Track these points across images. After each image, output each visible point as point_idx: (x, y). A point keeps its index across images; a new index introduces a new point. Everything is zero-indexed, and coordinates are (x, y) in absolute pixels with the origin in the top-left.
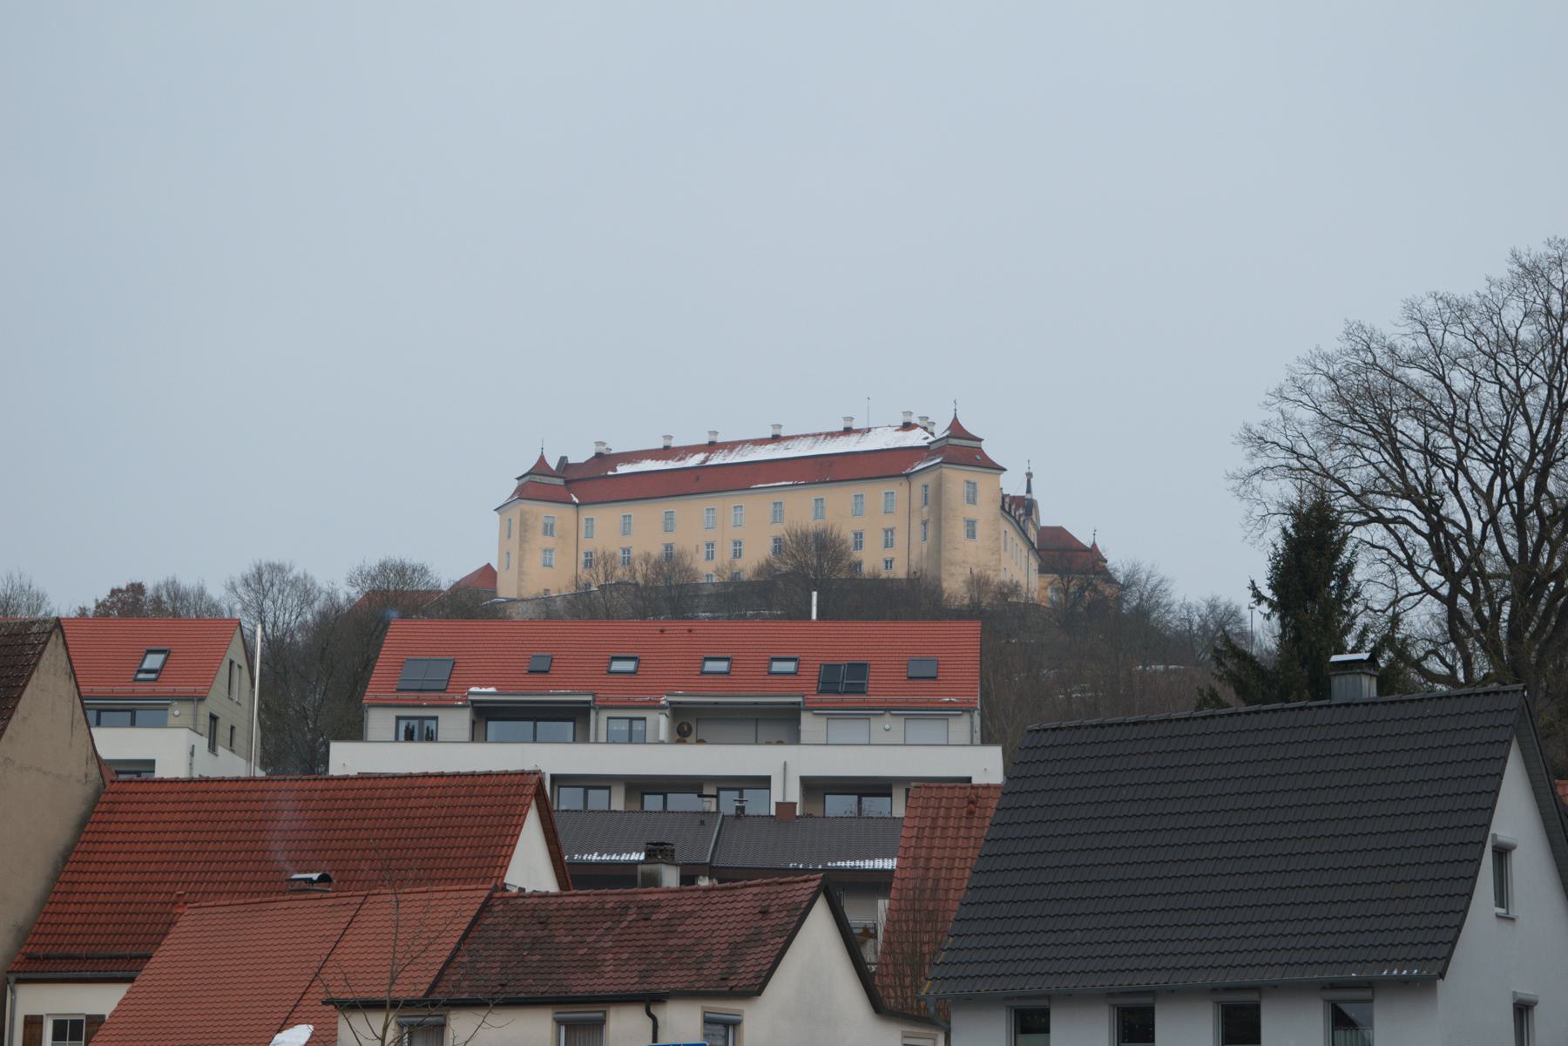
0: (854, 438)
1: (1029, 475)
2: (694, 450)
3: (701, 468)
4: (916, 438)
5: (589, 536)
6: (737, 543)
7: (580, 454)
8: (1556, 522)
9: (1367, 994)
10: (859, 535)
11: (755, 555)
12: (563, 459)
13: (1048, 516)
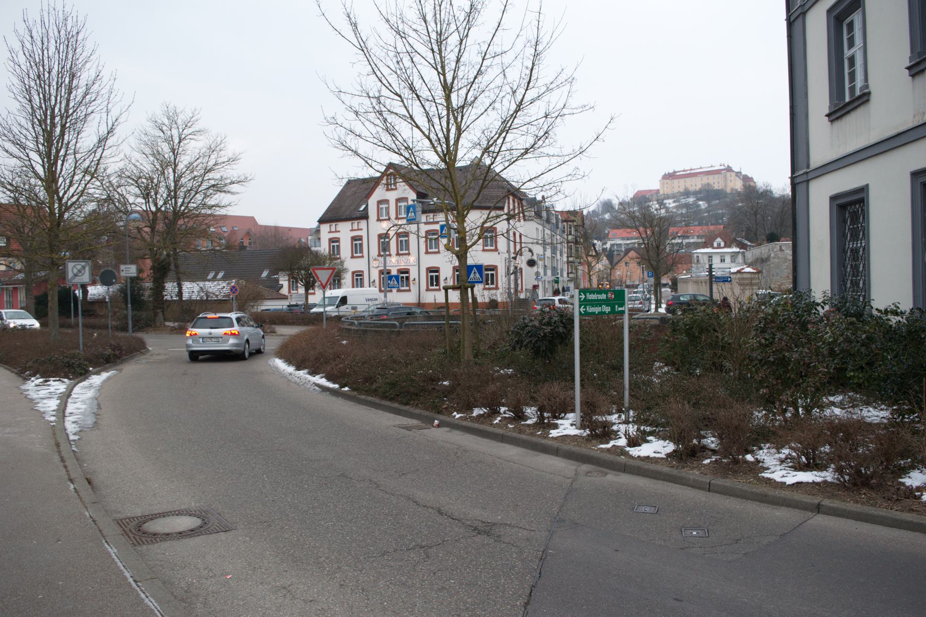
4: (722, 167)
7: (671, 171)
8: (596, 422)
9: (865, 98)
11: (698, 187)
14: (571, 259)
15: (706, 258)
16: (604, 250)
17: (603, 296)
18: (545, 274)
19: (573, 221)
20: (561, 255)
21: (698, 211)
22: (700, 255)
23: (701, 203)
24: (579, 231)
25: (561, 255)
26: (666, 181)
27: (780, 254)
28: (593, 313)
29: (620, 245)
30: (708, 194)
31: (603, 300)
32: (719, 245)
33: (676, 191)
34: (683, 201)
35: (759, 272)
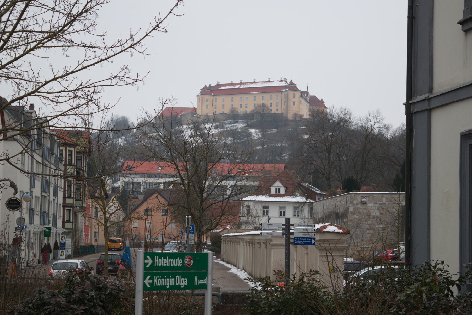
0: (270, 83)
1: (308, 86)
2: (237, 84)
3: (239, 89)
4: (283, 84)
5: (216, 102)
6: (246, 105)
7: (214, 84)
10: (271, 104)
11: (250, 109)
12: (210, 85)
13: (311, 94)
14: (69, 201)
15: (259, 209)
16: (114, 190)
17: (178, 262)
18: (31, 222)
19: (75, 145)
20: (55, 195)
21: (249, 141)
22: (252, 204)
23: (253, 131)
24: (86, 160)
25: (55, 195)
26: (206, 97)
27: (361, 209)
28: (164, 287)
29: (139, 183)
30: (262, 119)
31: (178, 268)
32: (278, 191)
33: (219, 111)
34: (229, 127)
35: (346, 233)
